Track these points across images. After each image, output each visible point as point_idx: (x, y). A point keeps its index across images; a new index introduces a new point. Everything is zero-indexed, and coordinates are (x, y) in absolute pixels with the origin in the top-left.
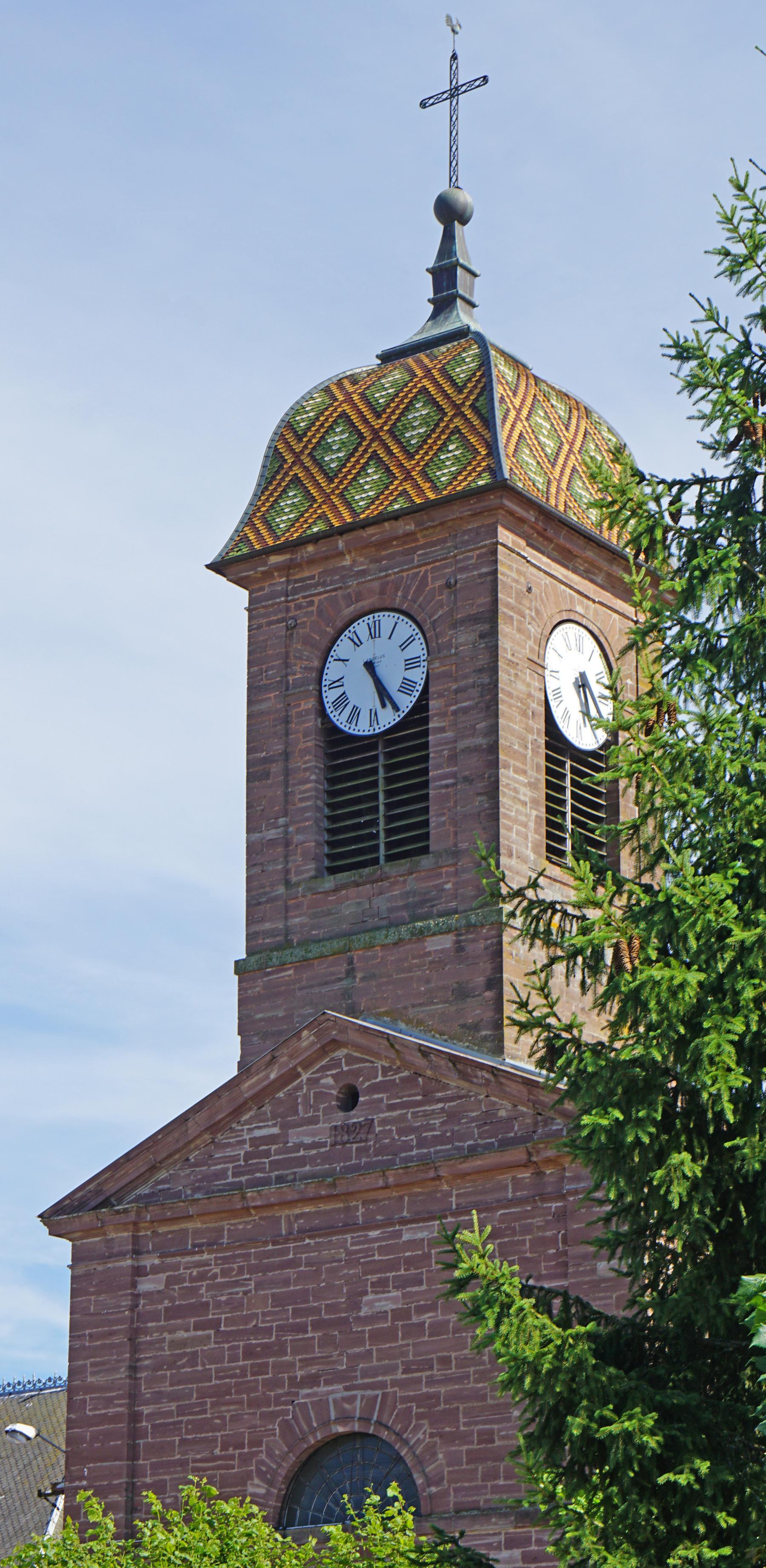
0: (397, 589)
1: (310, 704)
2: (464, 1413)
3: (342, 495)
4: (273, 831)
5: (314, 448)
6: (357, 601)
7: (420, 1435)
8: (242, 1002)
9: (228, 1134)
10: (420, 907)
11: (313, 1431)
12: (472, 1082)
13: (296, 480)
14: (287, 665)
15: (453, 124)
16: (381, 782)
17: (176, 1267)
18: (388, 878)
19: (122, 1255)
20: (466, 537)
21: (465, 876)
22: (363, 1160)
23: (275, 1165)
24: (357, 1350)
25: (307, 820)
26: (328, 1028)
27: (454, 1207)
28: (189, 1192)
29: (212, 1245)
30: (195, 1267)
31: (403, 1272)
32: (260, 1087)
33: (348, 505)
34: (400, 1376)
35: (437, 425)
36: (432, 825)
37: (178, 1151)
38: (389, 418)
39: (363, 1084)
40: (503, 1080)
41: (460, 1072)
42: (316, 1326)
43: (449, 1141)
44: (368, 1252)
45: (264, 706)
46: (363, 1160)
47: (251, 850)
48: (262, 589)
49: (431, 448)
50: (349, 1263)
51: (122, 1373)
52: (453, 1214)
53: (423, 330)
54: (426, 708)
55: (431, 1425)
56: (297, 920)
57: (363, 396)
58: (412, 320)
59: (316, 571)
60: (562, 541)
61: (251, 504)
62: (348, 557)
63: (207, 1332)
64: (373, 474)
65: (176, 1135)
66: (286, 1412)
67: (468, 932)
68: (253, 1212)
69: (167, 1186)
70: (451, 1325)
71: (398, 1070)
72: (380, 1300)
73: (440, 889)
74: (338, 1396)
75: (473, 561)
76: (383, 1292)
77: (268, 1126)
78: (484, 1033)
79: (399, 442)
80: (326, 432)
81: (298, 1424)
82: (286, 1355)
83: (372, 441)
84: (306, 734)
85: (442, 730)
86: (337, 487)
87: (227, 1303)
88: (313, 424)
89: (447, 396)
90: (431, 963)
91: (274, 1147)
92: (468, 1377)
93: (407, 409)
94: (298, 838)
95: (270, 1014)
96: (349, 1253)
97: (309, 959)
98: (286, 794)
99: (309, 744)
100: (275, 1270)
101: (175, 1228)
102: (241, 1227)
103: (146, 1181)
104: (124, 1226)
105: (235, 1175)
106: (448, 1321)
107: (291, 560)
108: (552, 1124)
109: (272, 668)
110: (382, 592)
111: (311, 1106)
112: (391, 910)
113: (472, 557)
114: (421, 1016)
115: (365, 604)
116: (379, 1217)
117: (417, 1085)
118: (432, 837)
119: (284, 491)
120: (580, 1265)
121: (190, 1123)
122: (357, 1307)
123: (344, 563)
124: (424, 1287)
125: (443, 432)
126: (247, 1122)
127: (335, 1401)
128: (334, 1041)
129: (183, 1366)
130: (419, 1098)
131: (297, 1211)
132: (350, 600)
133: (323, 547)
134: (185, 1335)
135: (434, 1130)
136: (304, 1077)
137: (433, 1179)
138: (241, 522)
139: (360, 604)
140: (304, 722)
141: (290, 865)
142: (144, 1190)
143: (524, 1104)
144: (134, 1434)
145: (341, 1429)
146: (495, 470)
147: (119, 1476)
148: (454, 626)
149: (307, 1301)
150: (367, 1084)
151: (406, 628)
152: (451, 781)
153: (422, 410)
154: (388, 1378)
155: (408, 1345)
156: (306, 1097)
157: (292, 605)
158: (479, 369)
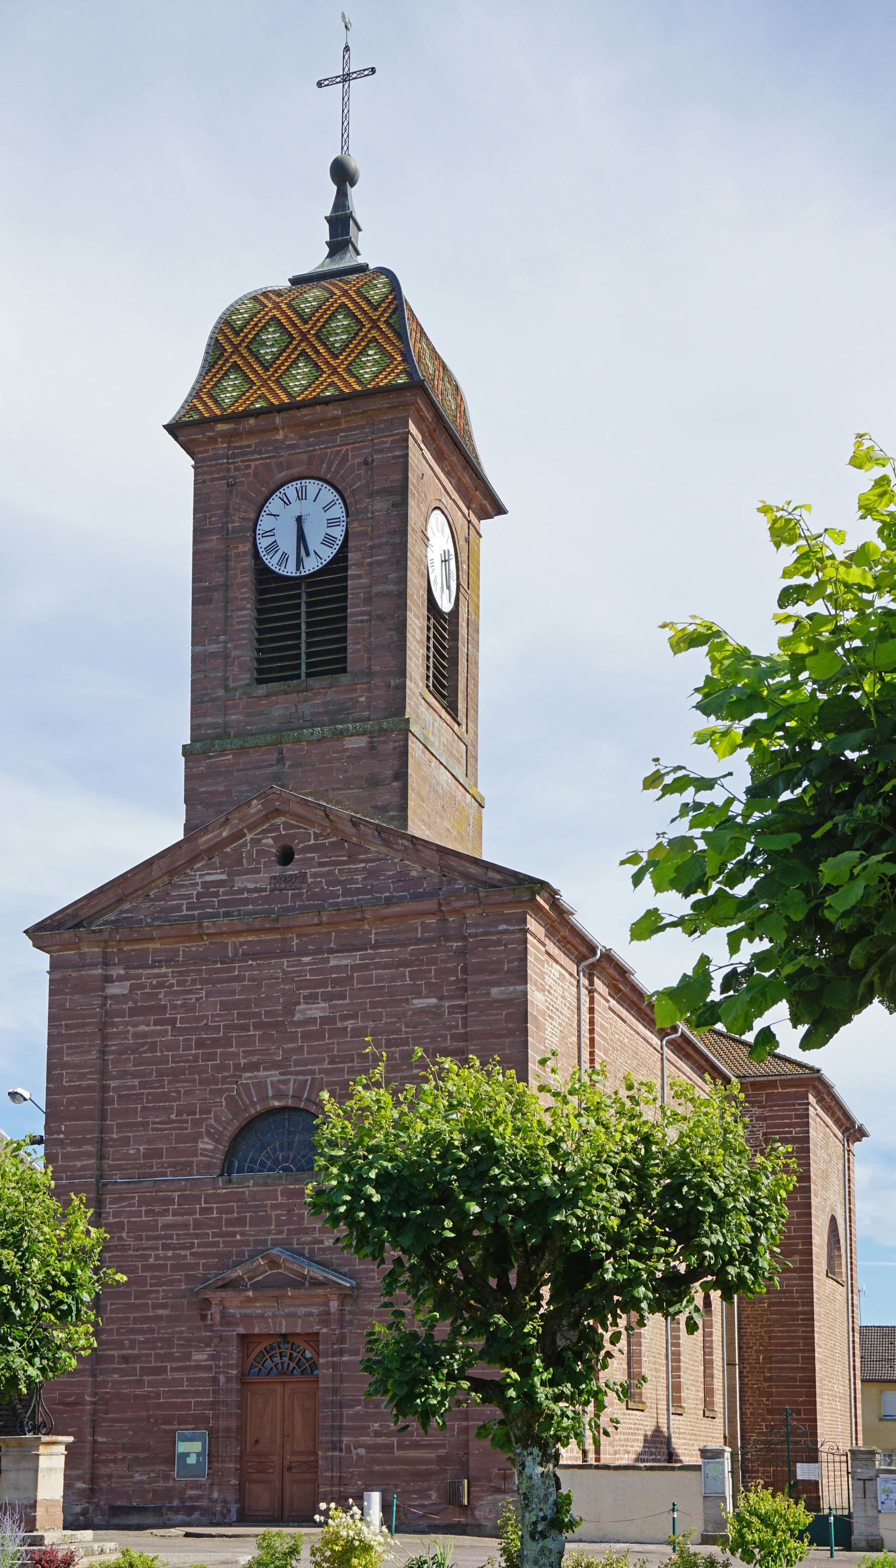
0: (322, 462)
1: (248, 547)
3: (277, 382)
4: (214, 646)
5: (250, 342)
6: (288, 468)
8: (188, 778)
9: (182, 877)
10: (337, 714)
11: (254, 1104)
12: (393, 849)
13: (235, 366)
14: (228, 515)
15: (345, 104)
16: (303, 615)
17: (139, 977)
18: (312, 689)
19: (94, 965)
21: (376, 692)
23: (223, 903)
24: (291, 1046)
26: (272, 800)
28: (149, 920)
29: (170, 961)
32: (213, 842)
33: (284, 389)
34: (326, 1066)
35: (357, 334)
36: (349, 651)
37: (142, 888)
38: (315, 324)
39: (297, 845)
40: (420, 848)
41: (383, 839)
42: (257, 1026)
43: (370, 892)
45: (207, 546)
47: (196, 659)
48: (207, 451)
49: (352, 351)
50: (285, 980)
51: (94, 1055)
52: (372, 948)
53: (323, 264)
54: (345, 559)
57: (289, 305)
58: (314, 256)
59: (253, 441)
60: (442, 444)
61: (197, 382)
64: (303, 368)
65: (142, 875)
66: (232, 1090)
71: (328, 836)
72: (310, 1009)
73: (355, 701)
74: (275, 1079)
79: (324, 344)
80: (261, 330)
81: (242, 1099)
83: (301, 341)
84: (243, 571)
85: (359, 577)
86: (273, 375)
87: (182, 1006)
88: (248, 323)
89: (365, 312)
91: (222, 890)
93: (330, 318)
96: (285, 973)
98: (226, 617)
99: (245, 579)
101: (138, 947)
103: (111, 911)
104: (97, 943)
105: (188, 909)
109: (215, 515)
110: (310, 462)
112: (314, 714)
114: (340, 797)
115: (295, 471)
118: (349, 660)
119: (226, 374)
121: (155, 867)
123: (278, 437)
124: (347, 1001)
125: (362, 340)
126: (198, 870)
127: (272, 1082)
128: (277, 810)
129: (145, 1052)
130: (345, 858)
131: (242, 939)
132: (281, 467)
133: (263, 421)
134: (147, 1029)
136: (249, 837)
137: (358, 920)
138: (190, 395)
139: (290, 472)
140: (241, 561)
142: (111, 917)
143: (432, 867)
144: (104, 1101)
145: (277, 1104)
146: (411, 373)
147: (91, 1132)
148: (371, 495)
151: (328, 494)
153: (342, 321)
154: (316, 1067)
156: (249, 853)
157: (232, 466)
158: (391, 293)
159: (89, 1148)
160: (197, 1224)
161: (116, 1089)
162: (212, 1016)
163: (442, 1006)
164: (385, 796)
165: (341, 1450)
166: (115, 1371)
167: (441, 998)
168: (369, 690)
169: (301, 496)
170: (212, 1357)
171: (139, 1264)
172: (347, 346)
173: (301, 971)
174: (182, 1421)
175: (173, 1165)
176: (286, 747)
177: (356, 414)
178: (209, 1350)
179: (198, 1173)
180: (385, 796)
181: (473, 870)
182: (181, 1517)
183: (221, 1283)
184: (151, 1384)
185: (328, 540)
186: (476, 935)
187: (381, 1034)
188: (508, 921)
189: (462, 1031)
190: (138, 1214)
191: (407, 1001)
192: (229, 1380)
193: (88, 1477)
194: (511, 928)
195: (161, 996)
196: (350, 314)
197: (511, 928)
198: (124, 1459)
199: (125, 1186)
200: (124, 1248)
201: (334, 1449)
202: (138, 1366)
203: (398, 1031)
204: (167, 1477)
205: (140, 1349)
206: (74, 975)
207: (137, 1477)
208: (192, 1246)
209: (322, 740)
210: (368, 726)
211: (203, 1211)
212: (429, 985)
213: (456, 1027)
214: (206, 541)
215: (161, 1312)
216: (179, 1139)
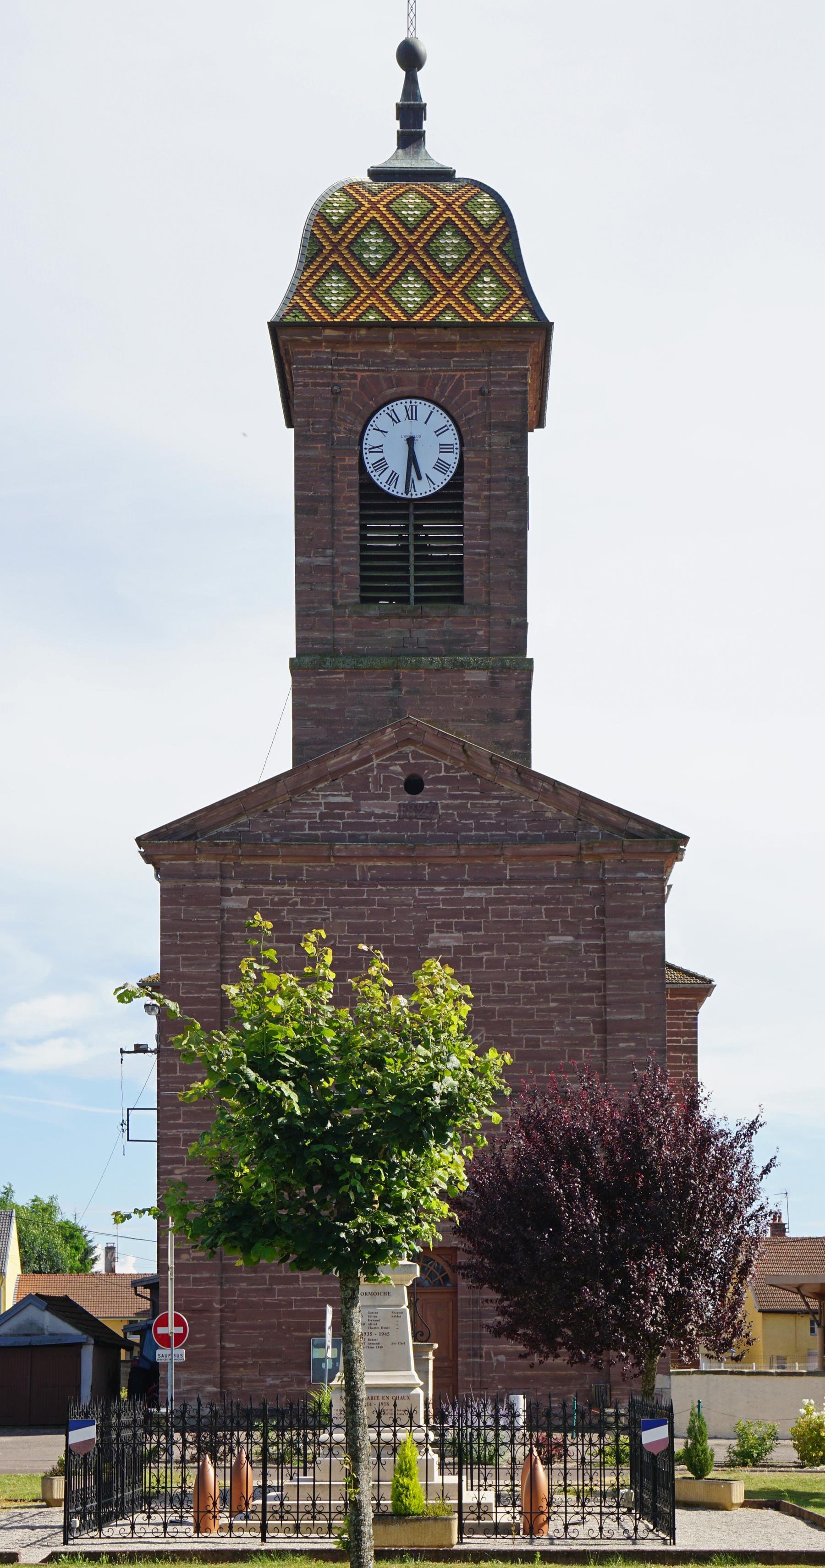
0: (435, 385)
1: (355, 461)
2: (514, 1025)
3: (387, 292)
4: (321, 559)
5: (351, 243)
6: (398, 386)
17: (259, 892)
18: (428, 617)
19: (213, 878)
20: (499, 358)
21: (497, 628)
25: (352, 555)
27: (508, 877)
28: (268, 836)
29: (291, 880)
30: (276, 895)
31: (464, 920)
32: (341, 765)
37: (262, 804)
41: (522, 779)
44: (433, 902)
45: (311, 453)
48: (309, 353)
54: (461, 486)
55: (487, 1031)
56: (344, 635)
59: (359, 350)
62: (391, 347)
63: (288, 945)
64: (412, 284)
67: (501, 672)
68: (332, 859)
69: (246, 829)
70: (505, 962)
71: (459, 770)
72: (444, 938)
73: (474, 634)
75: (506, 379)
76: (447, 933)
77: (341, 795)
78: (515, 751)
84: (350, 485)
85: (476, 509)
90: (468, 690)
91: (347, 812)
92: (519, 1000)
95: (323, 706)
96: (416, 900)
97: (359, 669)
98: (333, 531)
99: (353, 494)
100: (351, 905)
101: (257, 862)
102: (319, 869)
105: (310, 828)
106: (503, 959)
107: (344, 337)
108: (590, 828)
109: (319, 423)
110: (422, 382)
111: (381, 786)
113: (504, 376)
115: (406, 389)
116: (443, 877)
117: (476, 783)
119: (327, 273)
120: (615, 931)
122: (425, 940)
123: (386, 351)
124: (482, 933)
126: (321, 790)
131: (371, 864)
133: (374, 333)
135: (490, 819)
136: (375, 762)
139: (400, 389)
141: (336, 589)
148: (489, 427)
149: (381, 932)
150: (431, 776)
152: (483, 551)
155: (468, 973)
156: (376, 779)
157: (336, 373)
158: (501, 217)
162: (340, 937)
163: (578, 944)
165: (481, 1357)
166: (242, 1280)
167: (578, 937)
168: (489, 624)
169: (412, 415)
172: (459, 267)
176: (402, 672)
177: (474, 342)
180: (506, 733)
181: (614, 818)
185: (440, 466)
186: (615, 880)
187: (517, 967)
188: (645, 869)
189: (599, 969)
191: (543, 937)
193: (218, 1380)
195: (284, 913)
196: (458, 232)
197: (650, 876)
198: (255, 1364)
201: (475, 1356)
202: (267, 1275)
206: (188, 885)
207: (269, 1381)
209: (441, 669)
210: (490, 661)
213: (593, 965)
214: (309, 448)
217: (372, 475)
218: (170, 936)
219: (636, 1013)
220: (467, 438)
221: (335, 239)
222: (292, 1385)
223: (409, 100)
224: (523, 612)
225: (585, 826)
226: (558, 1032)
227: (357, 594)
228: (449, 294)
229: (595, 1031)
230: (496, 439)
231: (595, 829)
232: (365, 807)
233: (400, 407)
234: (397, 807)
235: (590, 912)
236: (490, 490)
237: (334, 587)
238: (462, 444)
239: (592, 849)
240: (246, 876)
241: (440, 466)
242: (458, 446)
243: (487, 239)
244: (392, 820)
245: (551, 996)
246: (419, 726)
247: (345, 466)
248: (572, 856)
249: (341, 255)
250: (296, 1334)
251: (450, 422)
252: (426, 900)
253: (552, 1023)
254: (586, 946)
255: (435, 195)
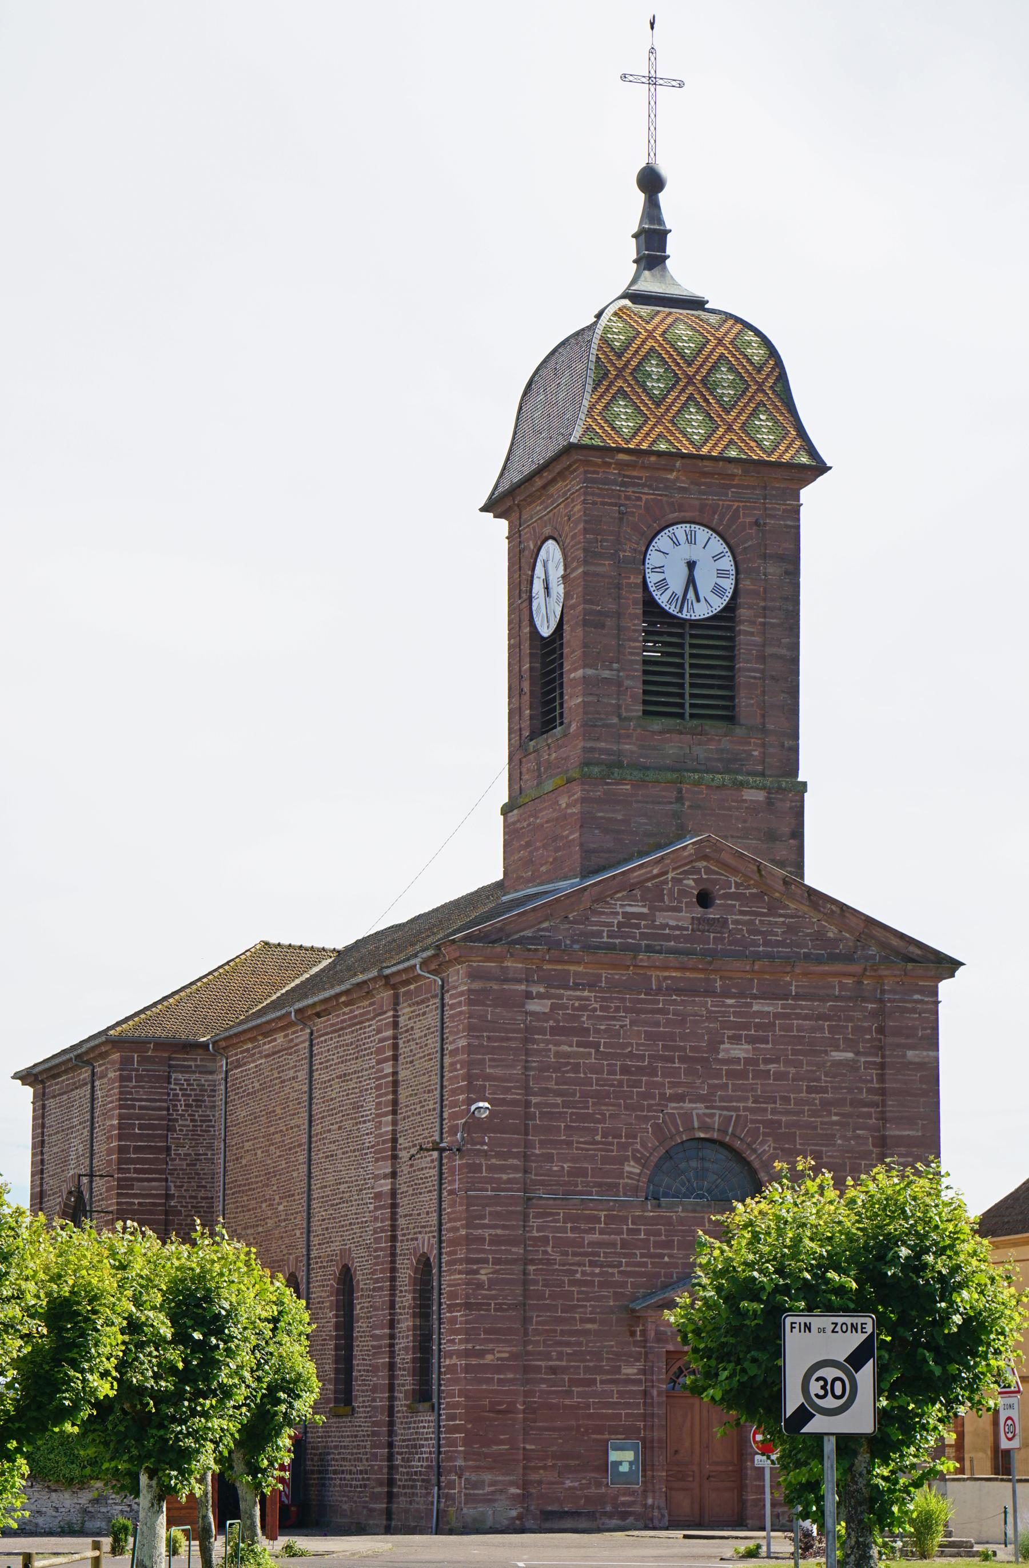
0: (715, 513)
1: (639, 580)
3: (672, 421)
4: (608, 672)
7: (766, 1147)
12: (819, 911)
19: (519, 981)
21: (771, 750)
22: (719, 947)
24: (716, 1082)
25: (636, 670)
28: (568, 942)
29: (592, 986)
30: (577, 1000)
34: (750, 1104)
39: (718, 891)
41: (810, 901)
42: (683, 1059)
46: (719, 947)
51: (518, 1070)
55: (775, 1141)
56: (627, 747)
59: (644, 474)
67: (777, 792)
71: (748, 887)
72: (735, 1049)
74: (701, 1112)
82: (657, 1076)
84: (635, 603)
85: (752, 634)
87: (605, 1031)
91: (643, 923)
92: (803, 1112)
94: (628, 683)
95: (611, 815)
96: (709, 1011)
97: (644, 781)
99: (638, 611)
101: (559, 967)
105: (609, 937)
106: (789, 1073)
109: (607, 541)
110: (702, 508)
115: (688, 515)
124: (770, 1046)
126: (619, 899)
127: (697, 1114)
129: (567, 1072)
130: (765, 910)
131: (667, 974)
133: (663, 461)
134: (569, 1049)
139: (682, 514)
141: (621, 702)
145: (702, 1135)
147: (517, 1146)
148: (764, 557)
152: (758, 675)
154: (741, 1105)
157: (623, 494)
159: (515, 1162)
160: (624, 1244)
161: (538, 1105)
164: (782, 851)
166: (543, 1381)
167: (857, 1053)
168: (763, 745)
170: (644, 1372)
171: (566, 1279)
173: (726, 1012)
174: (614, 1431)
175: (600, 1185)
176: (685, 787)
178: (639, 1365)
179: (625, 1195)
180: (782, 851)
181: (895, 942)
182: (615, 1522)
183: (661, 1303)
184: (580, 1395)
185: (718, 590)
186: (894, 1001)
187: (802, 1080)
189: (877, 1086)
190: (564, 1230)
191: (826, 1052)
192: (660, 1393)
193: (521, 1482)
194: (926, 999)
195: (584, 1019)
196: (731, 369)
197: (926, 999)
198: (554, 1466)
199: (551, 1202)
200: (549, 1262)
202: (566, 1377)
203: (818, 1080)
204: (599, 1484)
205: (568, 1361)
206: (495, 987)
207: (568, 1483)
208: (620, 1264)
209: (722, 787)
210: (768, 782)
211: (630, 1231)
212: (845, 1039)
213: (871, 1081)
215: (589, 1326)
216: (605, 1160)
217: (654, 594)
218: (477, 1037)
219: (913, 1130)
220: (743, 566)
221: (620, 364)
222: (590, 1488)
223: (654, 224)
224: (796, 736)
225: (863, 948)
226: (840, 1145)
227: (641, 708)
228: (729, 429)
229: (873, 1146)
230: (770, 570)
231: (873, 951)
232: (661, 918)
233: (680, 531)
234: (690, 921)
235: (869, 1030)
236: (765, 617)
237: (619, 699)
238: (737, 573)
239: (876, 970)
240: (548, 980)
241: (718, 590)
242: (734, 572)
243: (759, 378)
244: (685, 933)
245: (834, 1110)
246: (718, 844)
247: (630, 584)
248: (854, 976)
249: (626, 381)
250: (595, 1436)
251: (727, 549)
252: (719, 1012)
253: (834, 1136)
254: (865, 1062)
255: (705, 329)
